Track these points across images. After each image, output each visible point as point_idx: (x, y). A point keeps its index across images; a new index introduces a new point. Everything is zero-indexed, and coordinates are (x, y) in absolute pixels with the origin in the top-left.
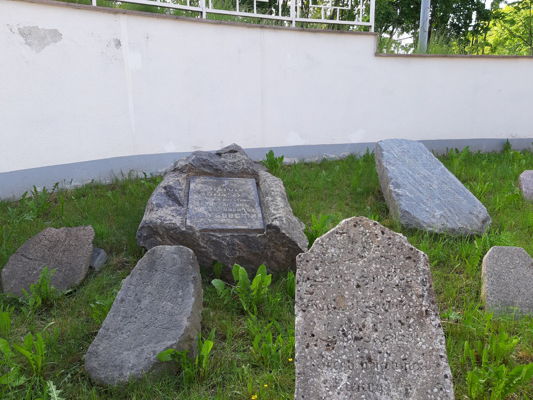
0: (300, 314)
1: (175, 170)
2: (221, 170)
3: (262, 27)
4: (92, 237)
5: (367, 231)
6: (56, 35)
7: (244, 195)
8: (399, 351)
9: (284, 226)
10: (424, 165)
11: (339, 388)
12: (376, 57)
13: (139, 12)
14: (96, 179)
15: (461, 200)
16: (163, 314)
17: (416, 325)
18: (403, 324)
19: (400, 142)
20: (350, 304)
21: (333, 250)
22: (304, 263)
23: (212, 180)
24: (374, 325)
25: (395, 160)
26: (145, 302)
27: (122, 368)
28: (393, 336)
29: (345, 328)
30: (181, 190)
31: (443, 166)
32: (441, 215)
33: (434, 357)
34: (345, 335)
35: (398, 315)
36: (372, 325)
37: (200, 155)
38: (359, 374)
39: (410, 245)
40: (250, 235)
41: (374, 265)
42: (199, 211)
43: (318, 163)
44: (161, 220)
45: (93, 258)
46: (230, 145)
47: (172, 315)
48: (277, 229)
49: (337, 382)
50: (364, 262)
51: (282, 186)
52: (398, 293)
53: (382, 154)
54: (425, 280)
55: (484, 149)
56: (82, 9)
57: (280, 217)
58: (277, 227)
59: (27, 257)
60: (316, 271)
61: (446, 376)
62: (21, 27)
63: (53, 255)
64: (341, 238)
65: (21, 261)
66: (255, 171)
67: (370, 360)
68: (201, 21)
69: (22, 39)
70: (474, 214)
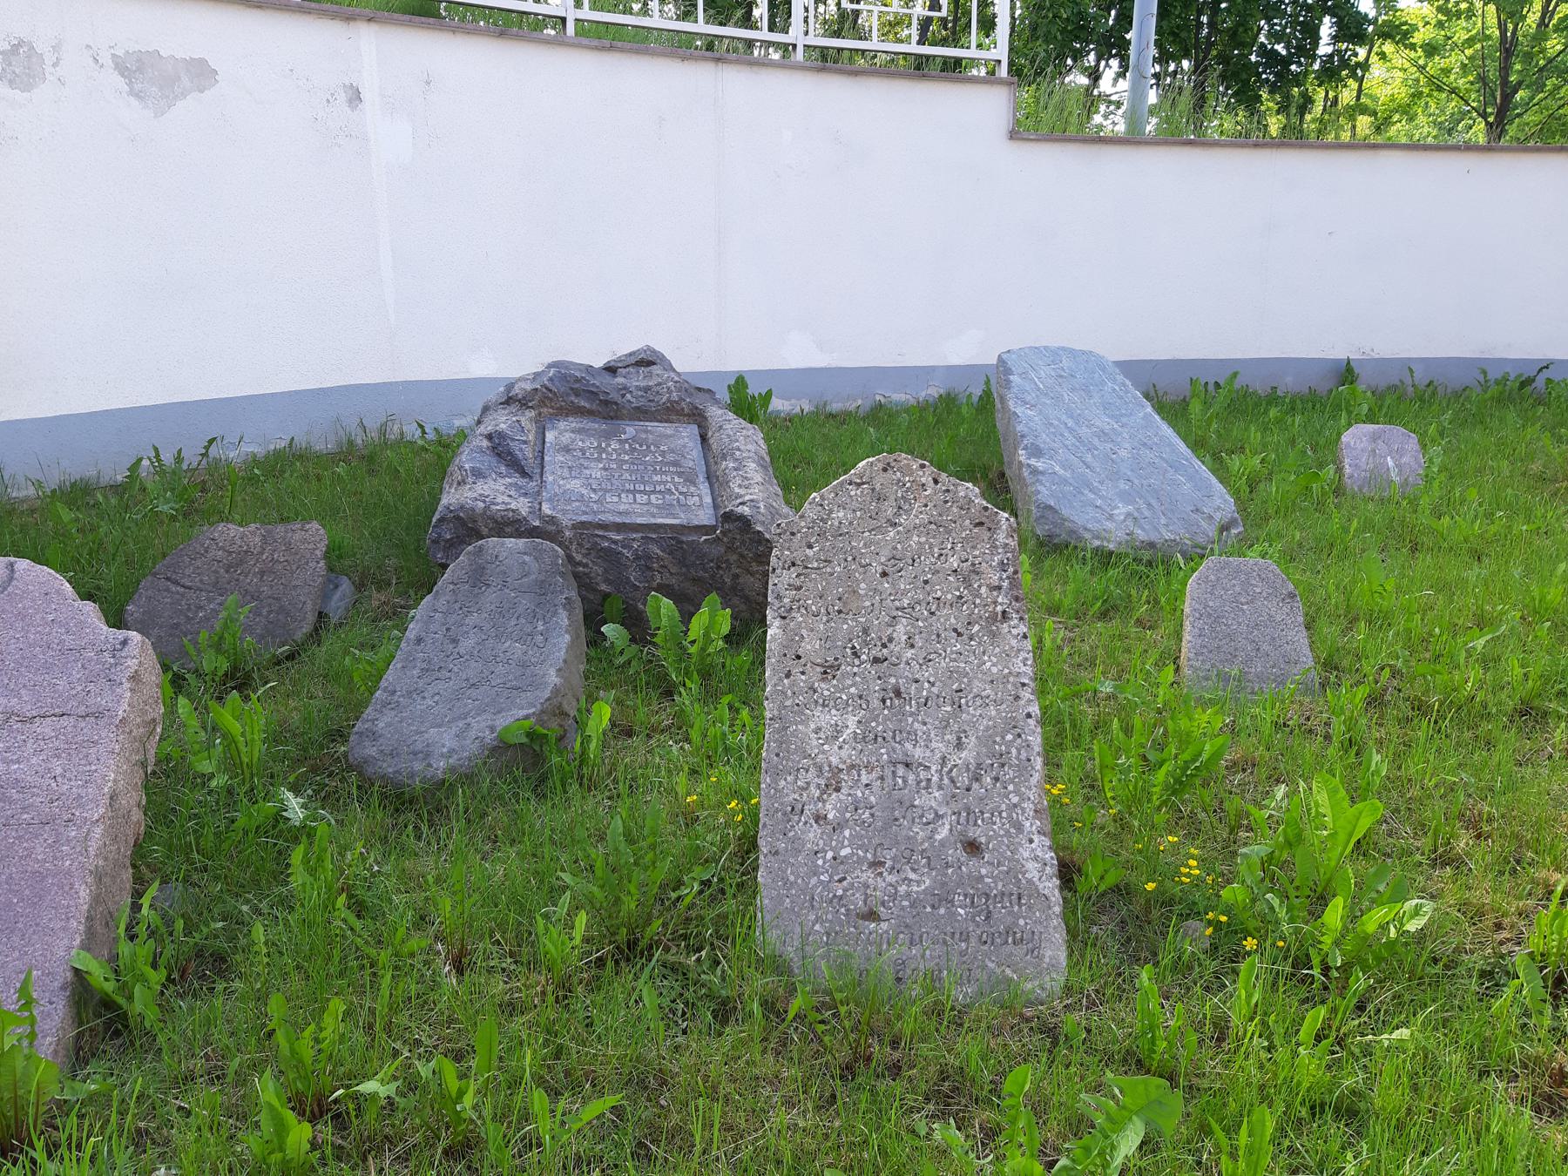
0: (777, 623)
1: (508, 401)
2: (616, 403)
3: (718, 60)
4: (322, 547)
5: (907, 479)
6: (202, 73)
7: (670, 457)
8: (950, 678)
9: (761, 518)
10: (1106, 406)
11: (841, 740)
12: (1012, 142)
13: (407, 17)
14: (302, 441)
15: (1179, 482)
16: (507, 663)
17: (984, 635)
18: (959, 635)
19: (1054, 355)
20: (868, 604)
21: (841, 514)
22: (787, 536)
23: (597, 426)
24: (909, 638)
25: (1037, 396)
26: (467, 644)
27: (428, 755)
28: (940, 655)
29: (856, 644)
30: (525, 442)
31: (1149, 409)
32: (1129, 515)
33: (1010, 686)
34: (856, 655)
35: (953, 620)
36: (905, 637)
37: (566, 368)
38: (878, 715)
39: (984, 502)
40: (684, 539)
41: (915, 538)
42: (568, 486)
43: (861, 413)
44: (484, 502)
45: (325, 596)
46: (640, 347)
47: (524, 665)
48: (744, 523)
49: (838, 730)
50: (898, 532)
51: (761, 442)
52: (955, 585)
53: (1008, 382)
54: (1005, 561)
55: (1289, 383)
56: (267, 8)
57: (752, 501)
58: (745, 517)
59: (178, 584)
60: (808, 550)
61: (1029, 716)
62: (120, 53)
63: (237, 580)
64: (858, 492)
65: (168, 590)
66: (697, 408)
67: (898, 693)
68: (560, 42)
69: (120, 82)
70: (1203, 513)
